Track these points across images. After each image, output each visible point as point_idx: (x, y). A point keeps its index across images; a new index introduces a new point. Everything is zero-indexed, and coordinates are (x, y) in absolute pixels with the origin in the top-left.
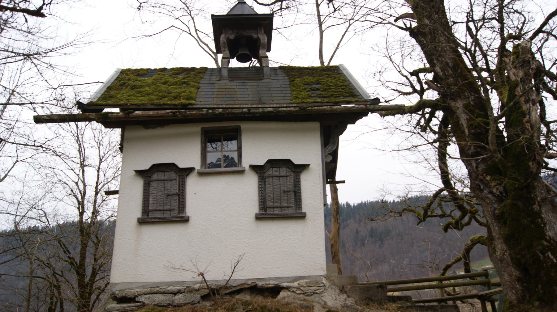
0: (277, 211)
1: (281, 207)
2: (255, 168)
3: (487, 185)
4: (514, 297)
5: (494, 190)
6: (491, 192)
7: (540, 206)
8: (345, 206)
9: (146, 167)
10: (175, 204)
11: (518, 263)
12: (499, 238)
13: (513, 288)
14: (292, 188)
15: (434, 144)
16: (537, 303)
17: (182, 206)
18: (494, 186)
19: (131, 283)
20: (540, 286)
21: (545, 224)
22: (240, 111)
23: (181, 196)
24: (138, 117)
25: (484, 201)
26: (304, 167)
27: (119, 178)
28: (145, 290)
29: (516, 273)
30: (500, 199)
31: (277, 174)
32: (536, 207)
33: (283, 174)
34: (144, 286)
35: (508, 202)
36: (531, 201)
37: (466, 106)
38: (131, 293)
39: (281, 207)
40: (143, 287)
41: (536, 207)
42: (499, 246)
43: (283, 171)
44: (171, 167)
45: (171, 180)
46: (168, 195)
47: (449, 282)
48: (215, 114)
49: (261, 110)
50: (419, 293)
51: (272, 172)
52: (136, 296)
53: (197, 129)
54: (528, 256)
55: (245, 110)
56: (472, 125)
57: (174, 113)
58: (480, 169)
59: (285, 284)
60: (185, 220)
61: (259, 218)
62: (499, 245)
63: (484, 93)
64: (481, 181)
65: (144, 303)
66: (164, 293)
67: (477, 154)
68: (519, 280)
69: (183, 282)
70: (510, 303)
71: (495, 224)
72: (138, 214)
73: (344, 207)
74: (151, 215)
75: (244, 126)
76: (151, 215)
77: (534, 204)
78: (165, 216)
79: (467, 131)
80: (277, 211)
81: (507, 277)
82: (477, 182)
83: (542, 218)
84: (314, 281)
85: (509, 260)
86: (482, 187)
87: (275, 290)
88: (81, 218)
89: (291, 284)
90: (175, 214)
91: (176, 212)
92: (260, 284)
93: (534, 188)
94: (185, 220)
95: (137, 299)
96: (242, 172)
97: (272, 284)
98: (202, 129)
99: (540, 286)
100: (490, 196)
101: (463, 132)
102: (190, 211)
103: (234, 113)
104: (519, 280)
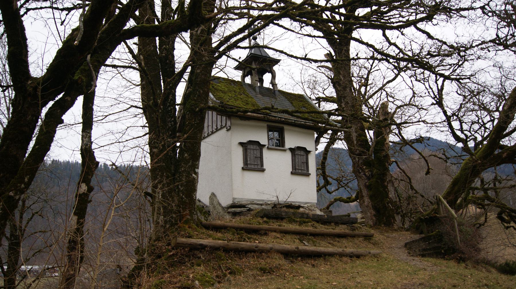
0: (300, 171)
1: (301, 170)
2: (291, 149)
3: (363, 170)
4: (372, 223)
5: (367, 174)
6: (365, 174)
7: (388, 183)
8: (103, 167)
9: (245, 141)
10: (259, 163)
11: (375, 208)
12: (367, 196)
13: (371, 219)
14: (305, 161)
16: (383, 225)
17: (262, 165)
18: (367, 172)
19: (242, 199)
20: (385, 218)
21: (389, 191)
22: (291, 121)
24: (248, 115)
25: (361, 178)
28: (249, 202)
29: (374, 212)
30: (369, 178)
31: (300, 153)
32: (386, 183)
33: (302, 154)
34: (248, 200)
35: (374, 180)
36: (383, 181)
38: (244, 203)
39: (301, 170)
40: (247, 201)
41: (386, 183)
42: (367, 200)
43: (255, 147)
44: (257, 143)
45: (257, 150)
46: (256, 157)
48: (280, 120)
49: (299, 122)
50: (514, 167)
51: (297, 152)
52: (246, 205)
53: (265, 124)
54: (381, 205)
55: (293, 121)
56: (359, 140)
57: (264, 117)
58: (360, 162)
59: (302, 205)
60: (263, 170)
61: (292, 173)
62: (367, 200)
64: (361, 168)
65: (250, 208)
66: (257, 204)
68: (375, 215)
69: (263, 200)
70: (370, 225)
71: (365, 190)
72: (241, 165)
73: (101, 168)
74: (249, 166)
75: (286, 127)
76: (249, 166)
77: (385, 182)
78: (255, 167)
79: (355, 142)
80: (300, 171)
81: (369, 214)
82: (358, 168)
83: (388, 189)
84: (312, 205)
85: (371, 206)
86: (360, 171)
87: (299, 207)
89: (304, 205)
90: (259, 167)
91: (260, 166)
92: (293, 204)
93: (386, 175)
94: (263, 170)
95: (246, 206)
96: (285, 150)
97: (297, 204)
98: (267, 125)
99: (385, 218)
100: (364, 176)
101: (353, 142)
103: (289, 122)
104: (375, 215)
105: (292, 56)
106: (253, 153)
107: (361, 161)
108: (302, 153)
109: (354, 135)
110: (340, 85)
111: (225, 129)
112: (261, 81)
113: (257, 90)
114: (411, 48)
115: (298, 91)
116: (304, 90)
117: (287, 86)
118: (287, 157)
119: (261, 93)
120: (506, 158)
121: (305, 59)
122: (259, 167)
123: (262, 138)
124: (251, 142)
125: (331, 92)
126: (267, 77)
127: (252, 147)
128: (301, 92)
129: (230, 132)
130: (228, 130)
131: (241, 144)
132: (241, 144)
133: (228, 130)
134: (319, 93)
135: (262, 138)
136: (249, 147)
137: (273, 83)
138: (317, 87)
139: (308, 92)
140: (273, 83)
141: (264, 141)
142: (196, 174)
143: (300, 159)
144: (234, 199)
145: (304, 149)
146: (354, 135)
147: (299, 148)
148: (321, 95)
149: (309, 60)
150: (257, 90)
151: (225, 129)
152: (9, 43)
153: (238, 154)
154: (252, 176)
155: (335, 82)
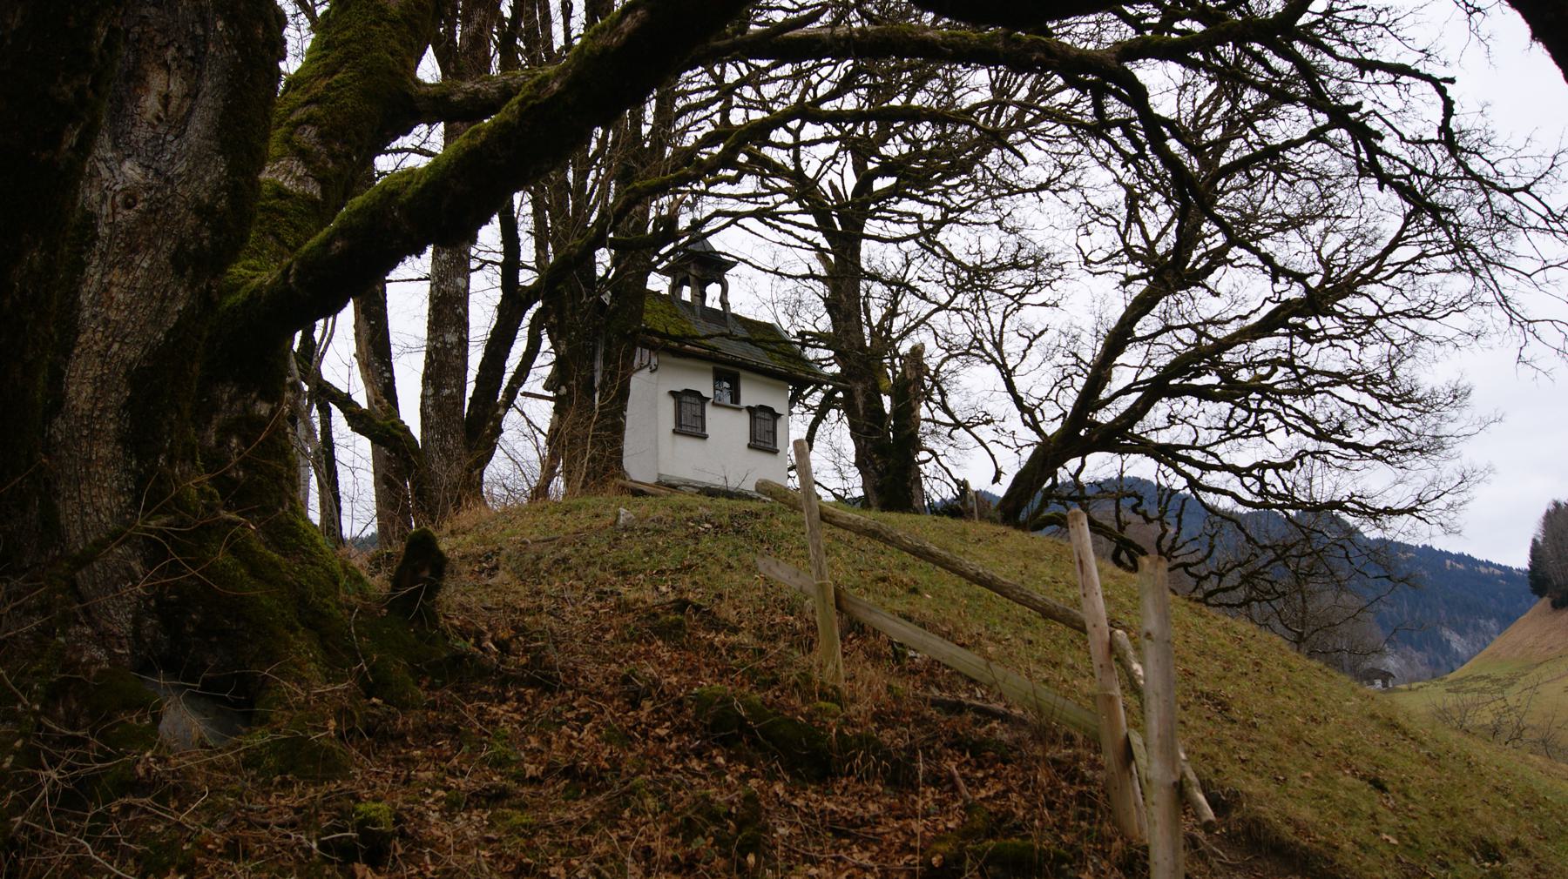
2: (749, 409)
3: (872, 461)
6: (875, 469)
9: (678, 389)
15: (1281, 471)
17: (704, 428)
23: (703, 417)
26: (780, 415)
27: (845, 418)
30: (881, 475)
32: (909, 484)
37: (864, 392)
41: (909, 484)
43: (693, 400)
44: (697, 394)
47: (1148, 147)
53: (710, 367)
60: (705, 437)
61: (749, 446)
63: (609, 188)
64: (868, 458)
67: (868, 434)
75: (743, 373)
76: (684, 429)
88: (1040, 432)
90: (699, 431)
94: (705, 437)
96: (740, 409)
98: (714, 369)
102: (707, 432)
105: (758, 268)
106: (690, 409)
107: (869, 446)
108: (767, 416)
109: (860, 401)
110: (840, 312)
111: (648, 369)
112: (703, 296)
113: (698, 310)
114: (1445, 128)
115: (765, 317)
116: (777, 317)
117: (743, 308)
118: (744, 420)
119: (703, 316)
120: (1097, 442)
121: (776, 272)
122: (699, 431)
123: (706, 387)
124: (688, 392)
125: (825, 323)
126: (713, 290)
127: (689, 399)
128: (769, 320)
129: (655, 375)
130: (652, 371)
131: (673, 393)
132: (673, 393)
133: (652, 371)
134: (805, 325)
135: (706, 387)
136: (684, 399)
137: (724, 301)
138: (802, 311)
139: (785, 323)
140: (724, 301)
141: (707, 391)
142: (625, 418)
143: (763, 426)
144: (660, 475)
145: (770, 410)
146: (860, 401)
147: (762, 408)
148: (809, 328)
149: (781, 274)
150: (698, 310)
151: (648, 369)
152: (1103, 388)
153: (667, 408)
154: (687, 445)
155: (831, 305)
